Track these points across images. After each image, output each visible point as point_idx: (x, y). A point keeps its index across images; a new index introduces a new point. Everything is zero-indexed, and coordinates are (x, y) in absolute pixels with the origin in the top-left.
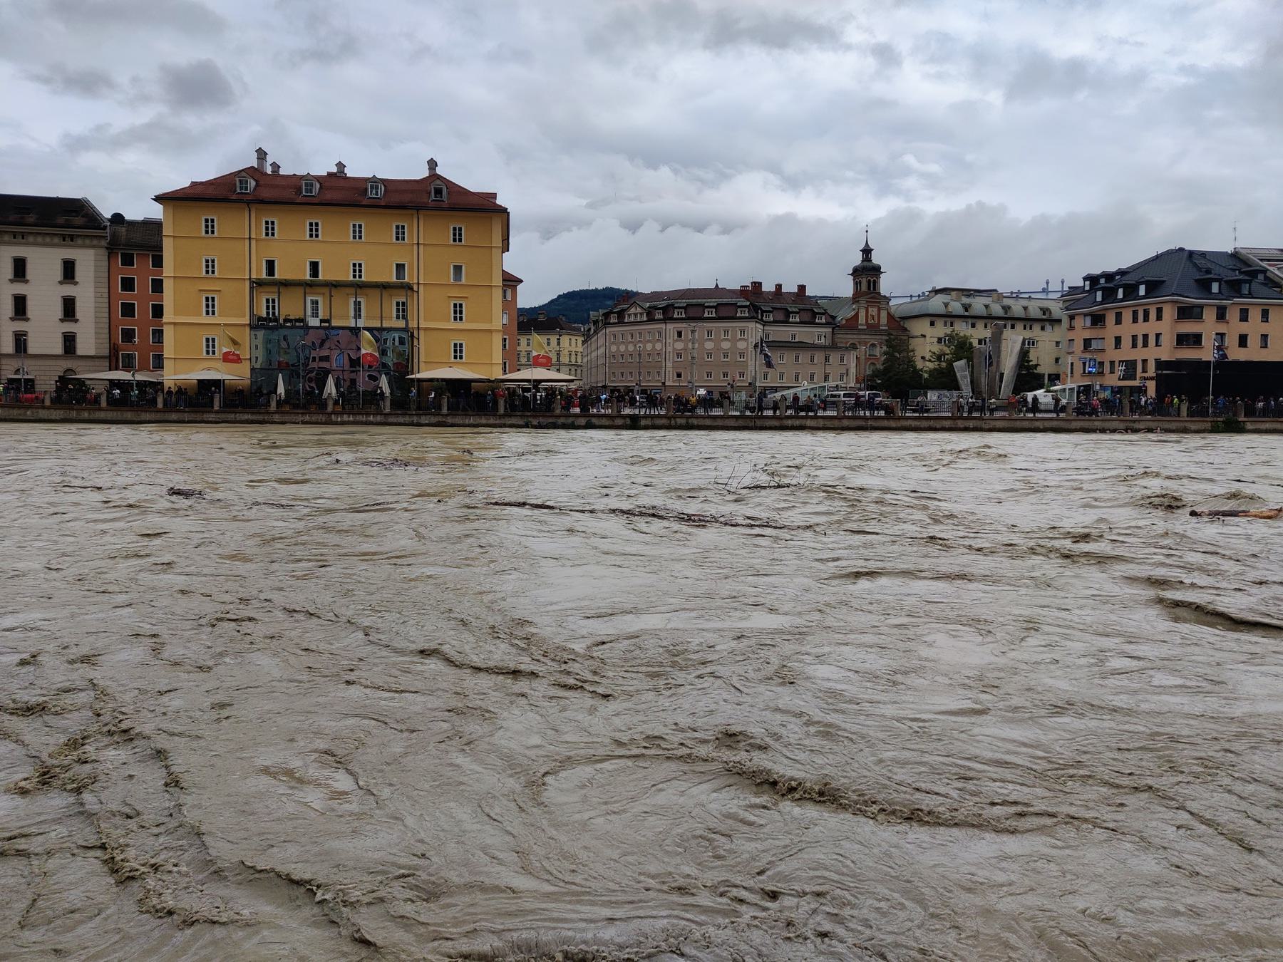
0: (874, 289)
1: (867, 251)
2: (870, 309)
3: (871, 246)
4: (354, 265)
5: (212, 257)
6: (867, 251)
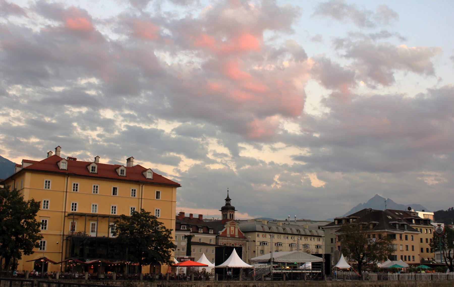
0: (232, 218)
1: (228, 200)
2: (231, 227)
3: (230, 197)
4: (73, 204)
5: (159, 209)
6: (228, 200)
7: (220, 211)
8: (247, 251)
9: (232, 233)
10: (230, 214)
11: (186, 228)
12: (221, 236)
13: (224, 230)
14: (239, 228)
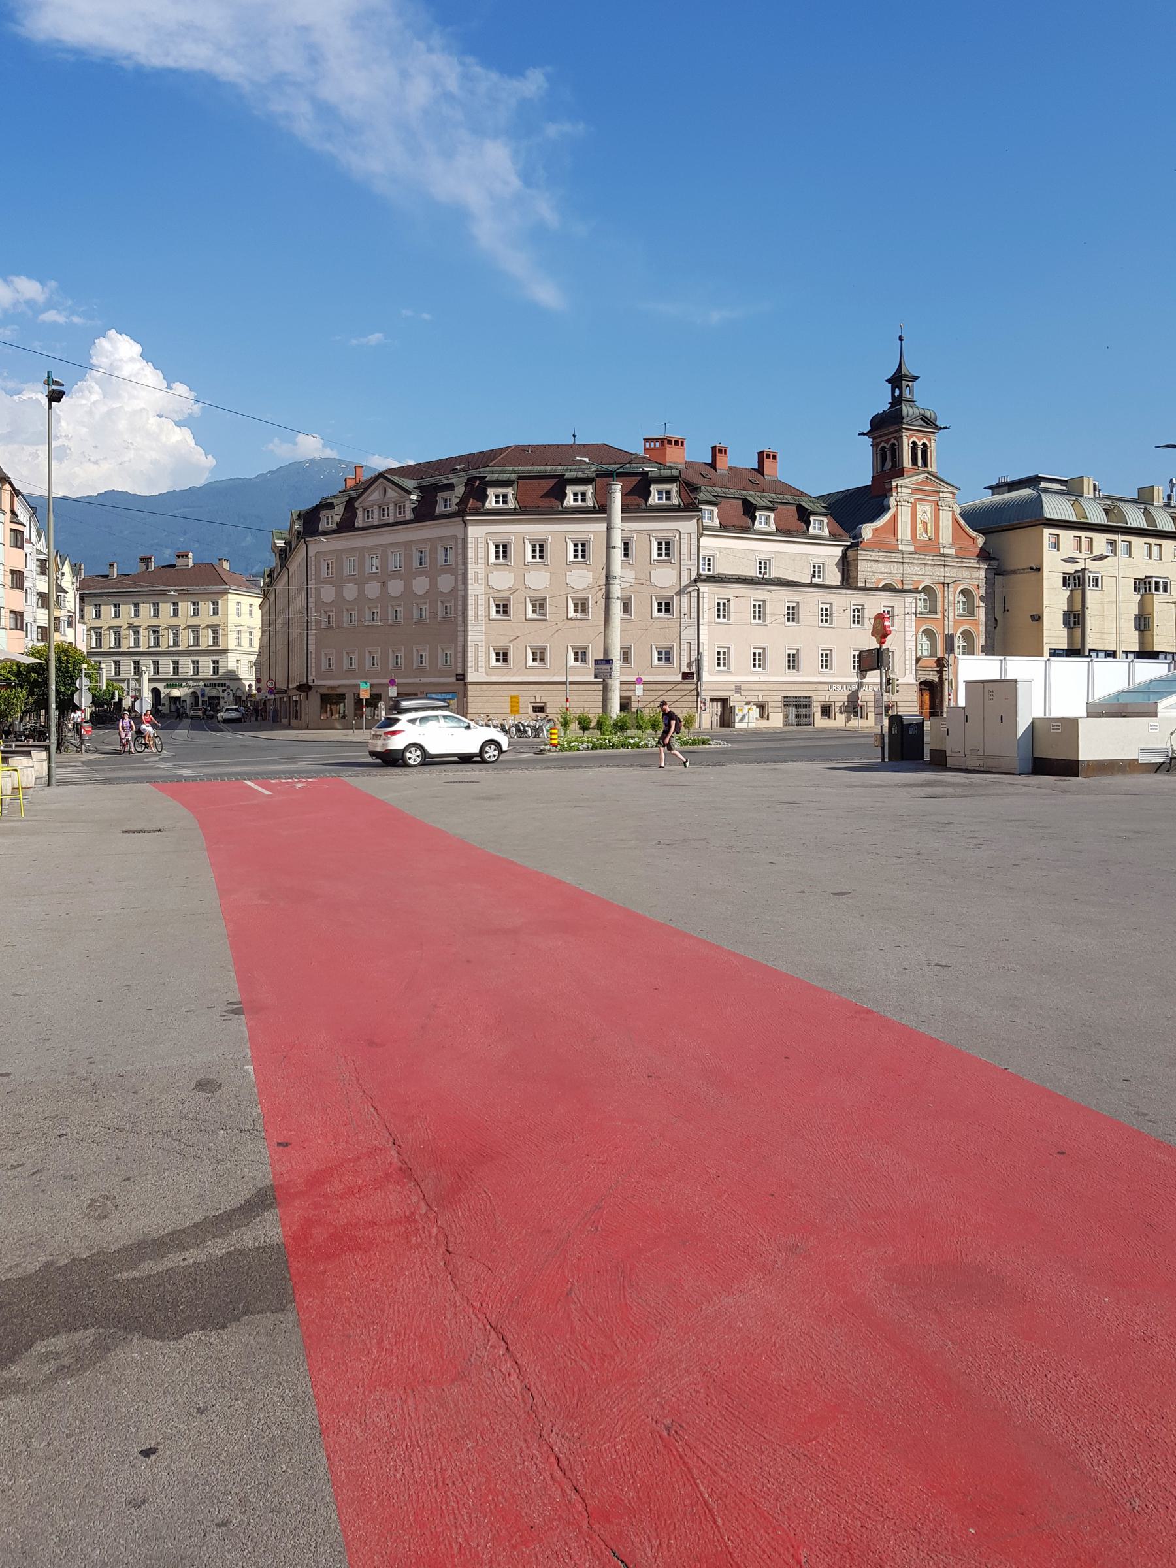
2: (920, 508)
7: (863, 434)
8: (996, 620)
9: (921, 536)
10: (914, 443)
11: (510, 498)
12: (876, 546)
13: (887, 516)
14: (957, 512)
